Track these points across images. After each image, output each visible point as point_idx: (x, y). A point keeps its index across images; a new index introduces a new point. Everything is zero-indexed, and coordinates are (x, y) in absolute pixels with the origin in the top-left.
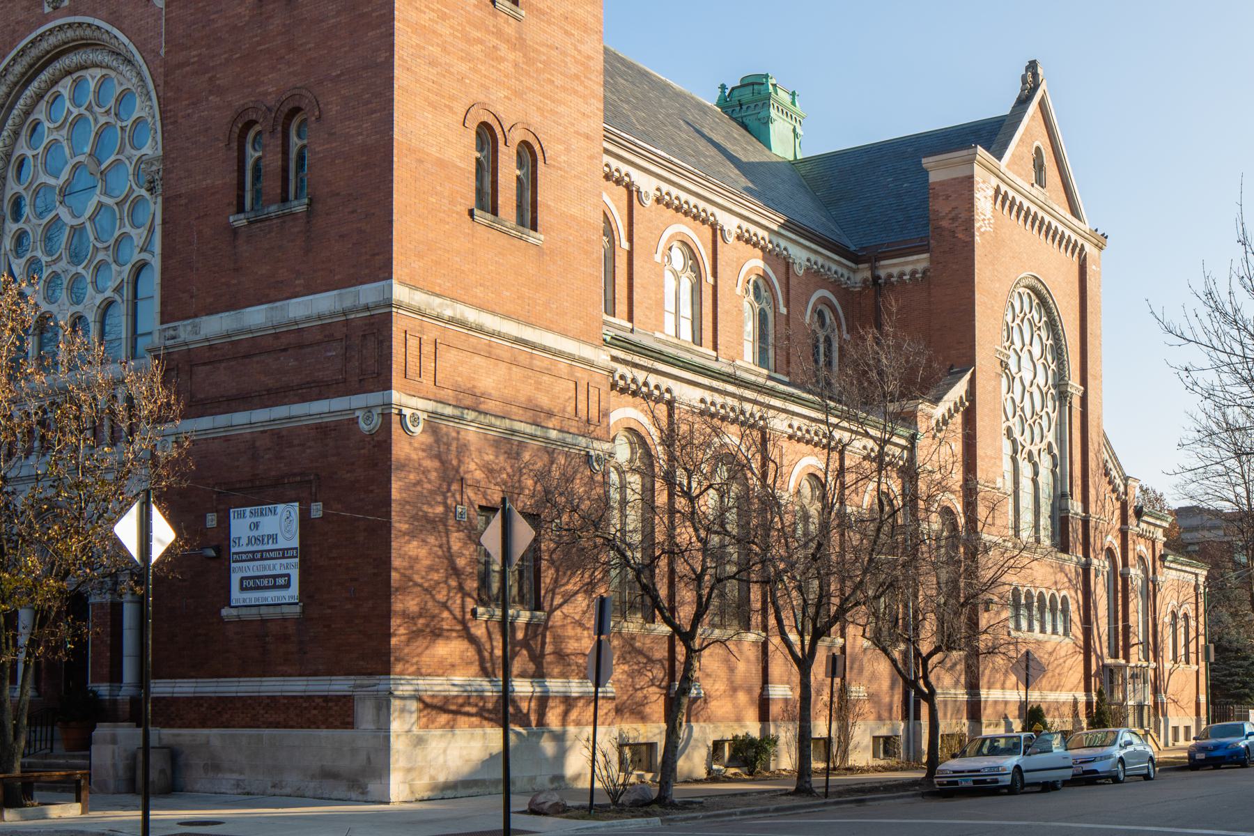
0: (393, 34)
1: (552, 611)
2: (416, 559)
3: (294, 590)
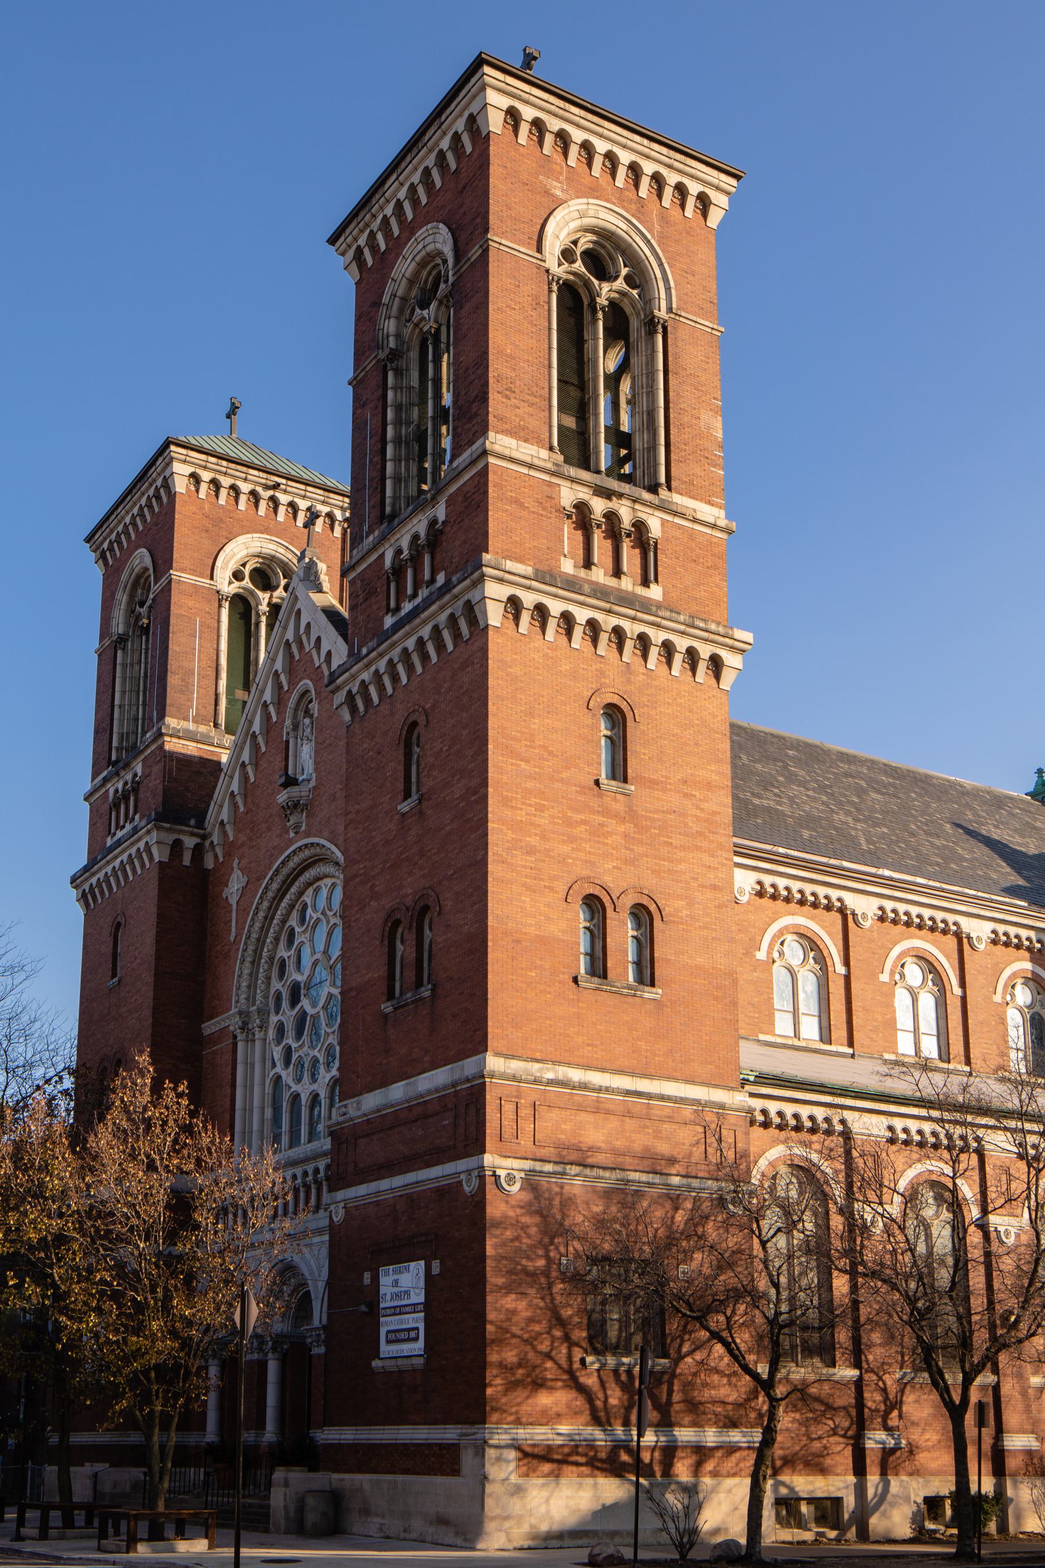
0: (487, 835)
1: (681, 1358)
2: (514, 1312)
3: (420, 1344)
